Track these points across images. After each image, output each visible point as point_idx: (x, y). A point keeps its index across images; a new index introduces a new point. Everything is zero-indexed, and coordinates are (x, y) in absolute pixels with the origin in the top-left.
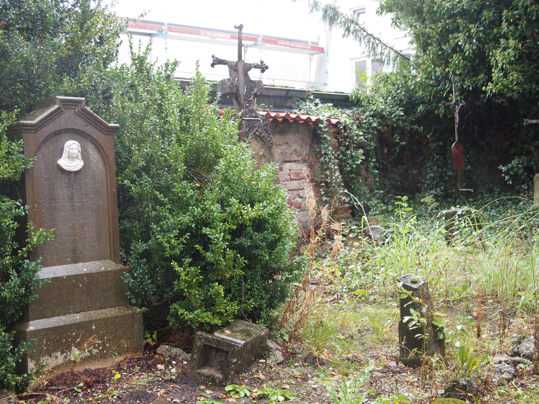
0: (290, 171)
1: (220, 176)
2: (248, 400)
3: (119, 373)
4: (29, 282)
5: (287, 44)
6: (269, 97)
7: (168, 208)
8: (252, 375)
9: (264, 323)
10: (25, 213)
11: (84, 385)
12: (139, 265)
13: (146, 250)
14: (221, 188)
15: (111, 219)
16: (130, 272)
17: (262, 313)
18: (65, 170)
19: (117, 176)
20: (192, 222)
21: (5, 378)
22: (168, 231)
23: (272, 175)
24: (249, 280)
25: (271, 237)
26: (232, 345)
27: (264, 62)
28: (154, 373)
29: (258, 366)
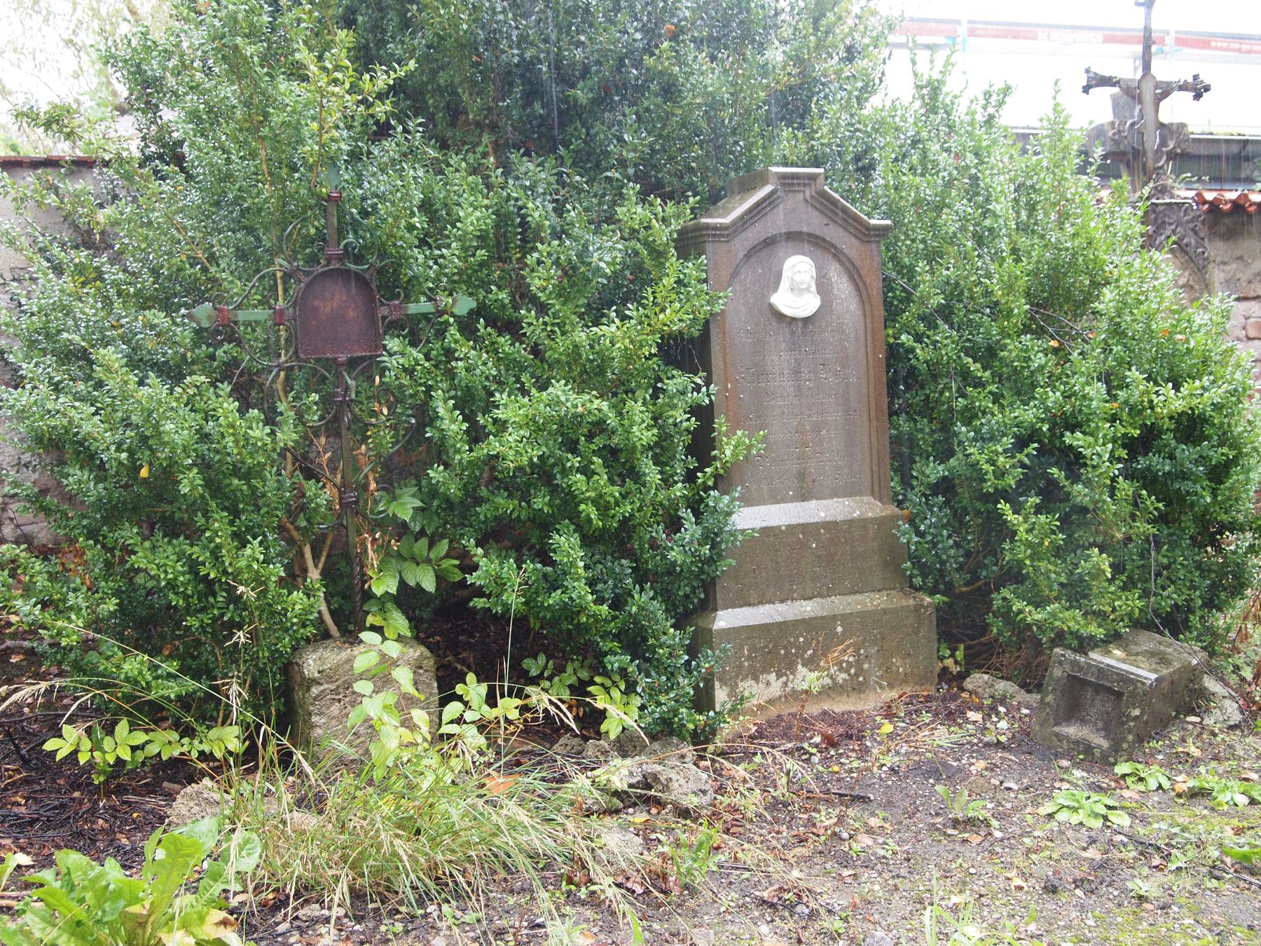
0: (1247, 318)
1: (1104, 325)
2: (1166, 797)
3: (891, 722)
4: (716, 534)
5: (1232, 45)
6: (1198, 157)
7: (990, 392)
8: (1172, 746)
9: (1198, 639)
10: (711, 400)
11: (823, 741)
12: (930, 508)
13: (944, 478)
14: (1107, 350)
15: (873, 414)
16: (911, 521)
17: (1192, 618)
18: (785, 316)
19: (886, 327)
20: (1043, 420)
21: (675, 716)
22: (992, 439)
23: (1220, 320)
24: (1166, 547)
25: (1218, 454)
26: (1131, 681)
27: (1201, 78)
28: (961, 728)
29: (1184, 729)
